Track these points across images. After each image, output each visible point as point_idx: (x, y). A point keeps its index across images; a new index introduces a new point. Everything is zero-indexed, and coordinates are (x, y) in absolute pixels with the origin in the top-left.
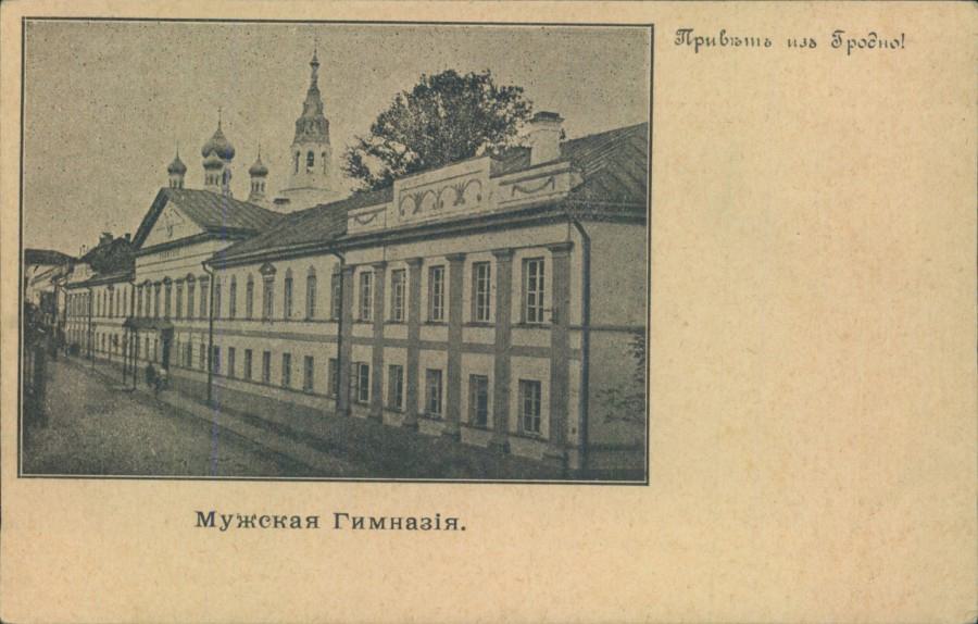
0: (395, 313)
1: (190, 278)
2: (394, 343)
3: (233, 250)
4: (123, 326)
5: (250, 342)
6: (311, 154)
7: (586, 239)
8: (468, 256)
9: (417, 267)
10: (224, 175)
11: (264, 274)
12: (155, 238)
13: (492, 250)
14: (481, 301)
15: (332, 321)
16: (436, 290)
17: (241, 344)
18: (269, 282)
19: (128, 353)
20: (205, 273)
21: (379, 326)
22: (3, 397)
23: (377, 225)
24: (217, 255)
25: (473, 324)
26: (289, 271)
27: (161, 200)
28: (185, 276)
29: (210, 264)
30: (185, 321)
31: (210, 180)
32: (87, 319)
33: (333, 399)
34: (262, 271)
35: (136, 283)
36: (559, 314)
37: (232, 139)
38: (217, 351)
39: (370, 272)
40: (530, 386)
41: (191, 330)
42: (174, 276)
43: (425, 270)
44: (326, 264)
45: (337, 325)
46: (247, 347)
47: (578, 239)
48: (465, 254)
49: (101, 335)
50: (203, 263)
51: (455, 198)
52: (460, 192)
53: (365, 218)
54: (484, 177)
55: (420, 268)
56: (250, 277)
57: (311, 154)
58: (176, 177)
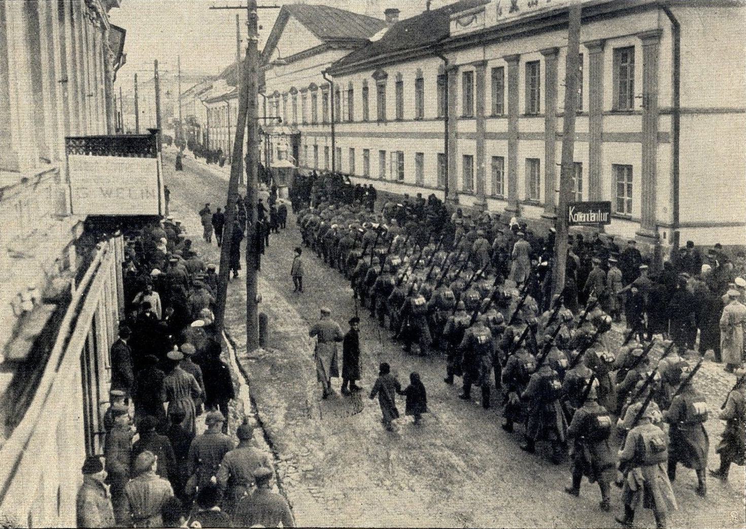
1: (313, 87)
2: (531, 136)
5: (366, 143)
7: (676, 28)
8: (522, 56)
9: (553, 57)
13: (540, 51)
14: (533, 97)
15: (438, 119)
16: (533, 83)
18: (381, 88)
21: (512, 116)
22: (429, 527)
23: (475, 26)
30: (321, 127)
33: (442, 190)
34: (375, 76)
35: (266, 94)
36: (649, 100)
38: (339, 150)
39: (472, 72)
41: (316, 135)
42: (298, 85)
43: (489, 69)
44: (431, 68)
45: (443, 123)
46: (350, 146)
50: (323, 73)
53: (465, 20)
55: (556, 59)
56: (365, 82)
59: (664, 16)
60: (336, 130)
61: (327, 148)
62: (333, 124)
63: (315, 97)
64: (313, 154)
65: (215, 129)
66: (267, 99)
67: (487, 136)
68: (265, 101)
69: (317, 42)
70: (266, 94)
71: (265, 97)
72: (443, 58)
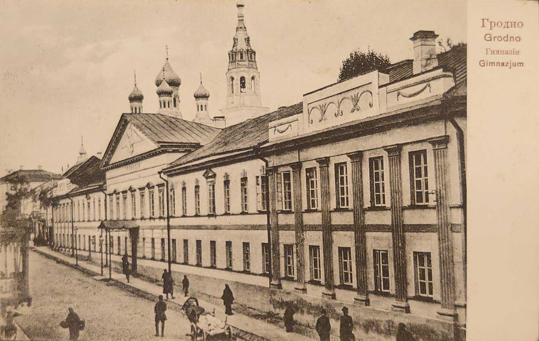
0: (152, 213)
3: (184, 160)
4: (99, 228)
6: (242, 79)
9: (358, 160)
10: (175, 99)
11: (207, 178)
12: (119, 155)
17: (192, 236)
19: (104, 250)
20: (163, 181)
24: (172, 165)
25: (412, 207)
26: (227, 176)
27: (123, 122)
28: (146, 185)
29: (165, 173)
31: (163, 105)
32: (70, 224)
35: (107, 192)
37: (179, 73)
40: (314, 249)
41: (152, 228)
42: (136, 185)
47: (452, 131)
48: (329, 158)
49: (82, 237)
50: (159, 173)
51: (352, 106)
52: (356, 100)
54: (374, 88)
57: (242, 79)
58: (136, 104)
59: (450, 125)
60: (171, 224)
61: (163, 240)
62: (169, 218)
63: (118, 199)
64: (150, 245)
65: (59, 224)
66: (108, 196)
67: (279, 227)
68: (106, 197)
69: (153, 146)
70: (107, 192)
71: (106, 195)
72: (265, 161)
